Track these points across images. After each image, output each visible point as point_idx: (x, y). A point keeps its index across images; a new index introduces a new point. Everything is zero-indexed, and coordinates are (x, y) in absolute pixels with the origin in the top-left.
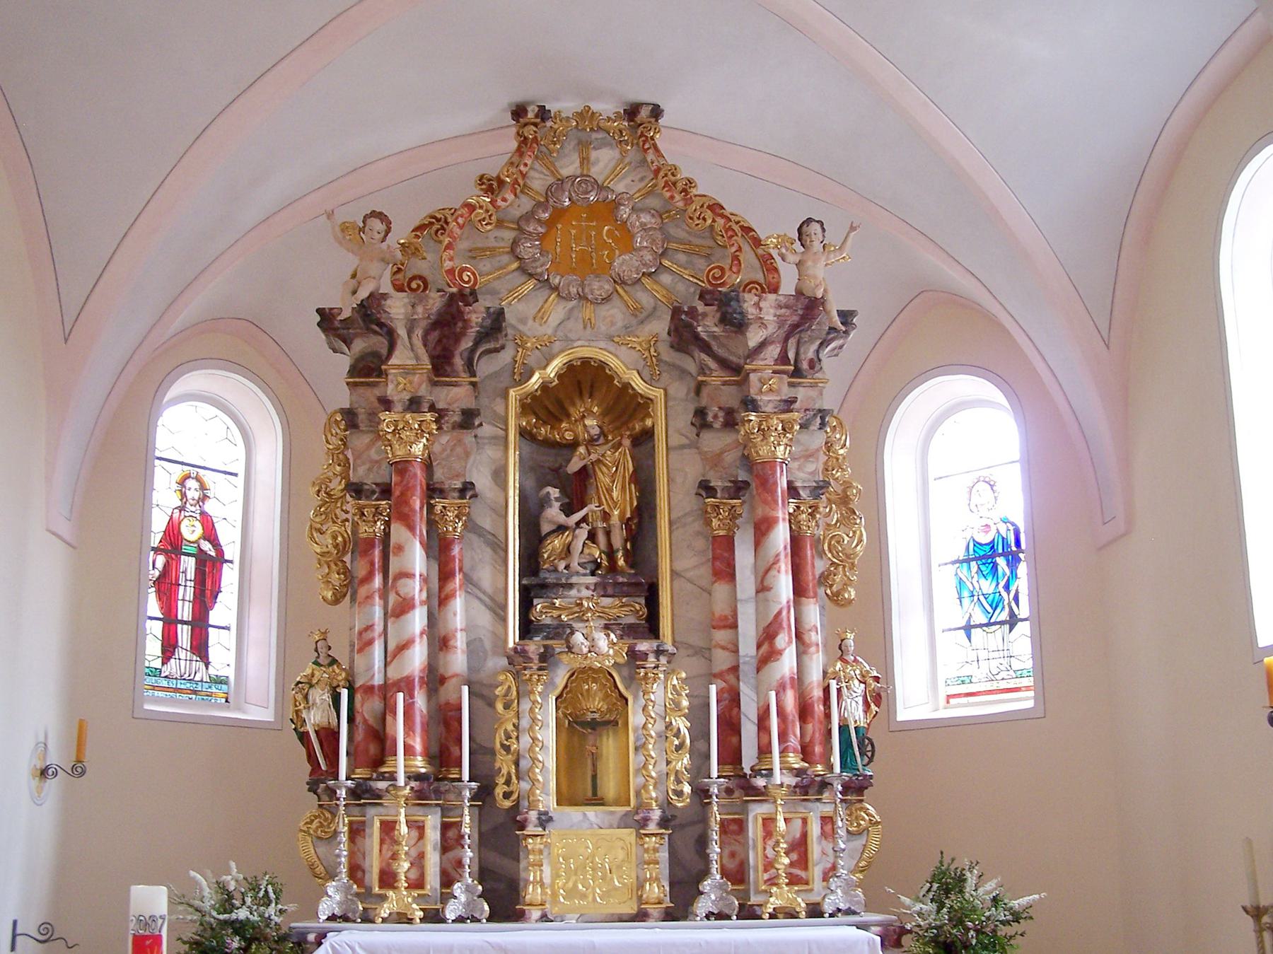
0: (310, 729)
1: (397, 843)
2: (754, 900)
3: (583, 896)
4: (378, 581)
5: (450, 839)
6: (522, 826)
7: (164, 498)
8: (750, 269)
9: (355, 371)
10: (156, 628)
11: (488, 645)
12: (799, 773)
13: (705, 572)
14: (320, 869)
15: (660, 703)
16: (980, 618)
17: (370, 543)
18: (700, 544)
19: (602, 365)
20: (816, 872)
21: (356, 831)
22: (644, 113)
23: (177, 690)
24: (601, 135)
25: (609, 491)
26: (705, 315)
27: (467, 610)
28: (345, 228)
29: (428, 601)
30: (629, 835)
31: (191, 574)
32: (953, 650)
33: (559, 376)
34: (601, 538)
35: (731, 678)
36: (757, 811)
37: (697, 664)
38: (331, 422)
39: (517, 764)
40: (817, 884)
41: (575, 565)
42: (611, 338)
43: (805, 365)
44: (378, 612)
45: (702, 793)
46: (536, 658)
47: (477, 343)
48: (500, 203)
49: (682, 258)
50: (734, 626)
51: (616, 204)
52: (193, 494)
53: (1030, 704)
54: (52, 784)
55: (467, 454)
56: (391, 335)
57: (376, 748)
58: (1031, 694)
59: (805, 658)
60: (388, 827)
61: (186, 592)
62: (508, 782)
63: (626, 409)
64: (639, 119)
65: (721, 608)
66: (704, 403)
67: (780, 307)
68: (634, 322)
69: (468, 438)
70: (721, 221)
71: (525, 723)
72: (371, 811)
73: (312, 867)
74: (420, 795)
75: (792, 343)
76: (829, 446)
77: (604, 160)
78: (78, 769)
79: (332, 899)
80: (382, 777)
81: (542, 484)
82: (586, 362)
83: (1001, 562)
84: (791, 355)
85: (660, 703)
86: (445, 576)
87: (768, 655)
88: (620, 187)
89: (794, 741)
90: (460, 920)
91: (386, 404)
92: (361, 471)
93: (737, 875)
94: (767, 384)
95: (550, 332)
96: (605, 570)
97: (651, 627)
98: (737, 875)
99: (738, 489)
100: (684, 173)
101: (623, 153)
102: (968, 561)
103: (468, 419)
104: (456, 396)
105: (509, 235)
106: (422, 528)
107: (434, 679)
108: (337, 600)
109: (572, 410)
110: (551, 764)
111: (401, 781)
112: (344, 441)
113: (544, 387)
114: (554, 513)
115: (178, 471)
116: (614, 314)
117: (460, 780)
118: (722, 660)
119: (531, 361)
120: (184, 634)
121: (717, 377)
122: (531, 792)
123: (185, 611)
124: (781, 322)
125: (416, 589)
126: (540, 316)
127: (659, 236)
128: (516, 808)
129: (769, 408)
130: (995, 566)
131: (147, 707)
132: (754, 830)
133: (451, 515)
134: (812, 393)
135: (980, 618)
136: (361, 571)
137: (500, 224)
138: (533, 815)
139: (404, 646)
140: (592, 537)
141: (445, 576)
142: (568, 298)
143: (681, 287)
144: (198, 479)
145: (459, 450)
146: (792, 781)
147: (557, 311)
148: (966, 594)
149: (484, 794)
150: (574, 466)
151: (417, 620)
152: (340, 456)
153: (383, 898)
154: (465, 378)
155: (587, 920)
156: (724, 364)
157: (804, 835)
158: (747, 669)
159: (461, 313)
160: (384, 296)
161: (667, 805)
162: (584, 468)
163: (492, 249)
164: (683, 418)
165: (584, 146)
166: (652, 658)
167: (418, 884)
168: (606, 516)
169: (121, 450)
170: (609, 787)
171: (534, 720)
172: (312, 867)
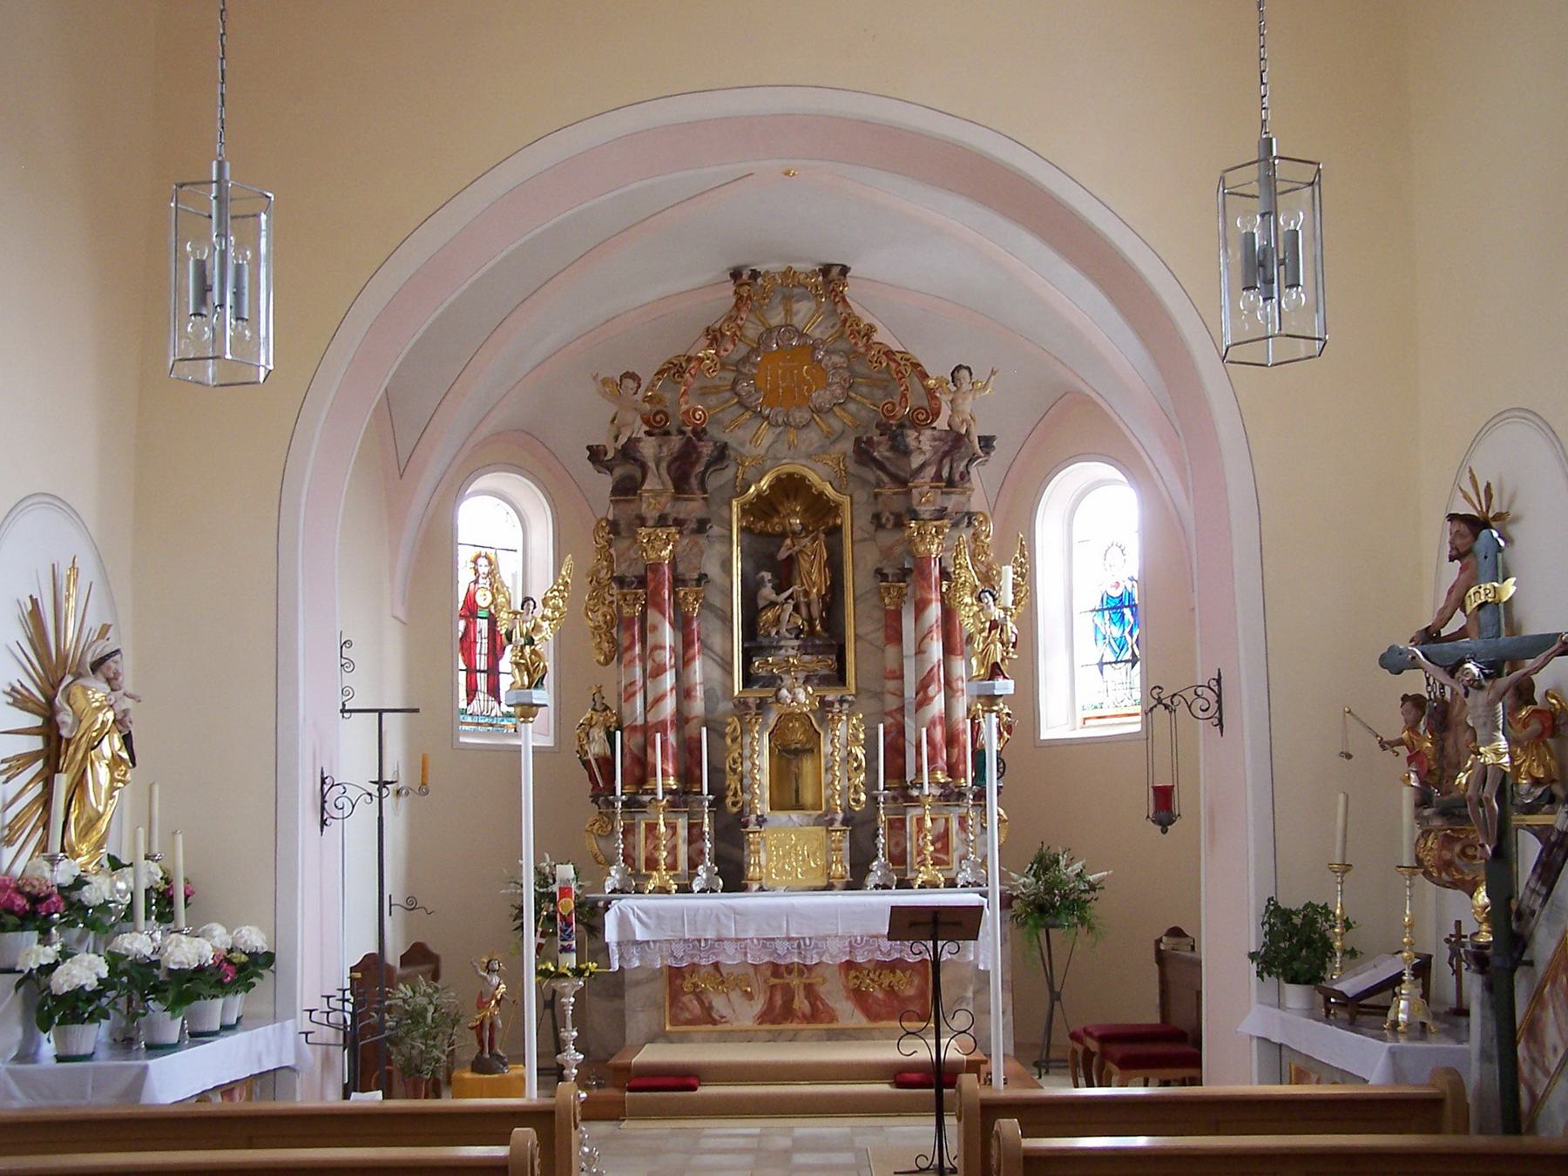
0: (590, 756)
1: (658, 838)
2: (909, 876)
3: (789, 874)
4: (637, 649)
5: (695, 835)
6: (746, 826)
7: (465, 577)
8: (916, 399)
9: (615, 491)
10: (462, 677)
11: (719, 693)
12: (943, 786)
13: (879, 637)
14: (601, 858)
15: (844, 740)
16: (1110, 657)
17: (631, 621)
18: (878, 614)
19: (803, 478)
20: (955, 856)
21: (629, 831)
22: (835, 271)
23: (478, 724)
24: (801, 290)
25: (809, 574)
26: (879, 443)
27: (703, 667)
28: (605, 382)
29: (676, 666)
30: (821, 830)
31: (485, 633)
32: (1088, 678)
33: (770, 487)
34: (804, 610)
35: (899, 717)
36: (912, 814)
37: (872, 705)
38: (598, 527)
39: (741, 781)
40: (955, 865)
41: (783, 631)
42: (809, 456)
43: (957, 477)
44: (638, 671)
45: (873, 800)
46: (753, 707)
47: (707, 469)
48: (722, 353)
49: (864, 390)
50: (901, 677)
51: (814, 348)
52: (484, 569)
53: (1138, 728)
54: (402, 800)
55: (702, 552)
56: (644, 467)
57: (641, 771)
58: (1139, 718)
59: (954, 701)
60: (652, 828)
61: (482, 646)
62: (735, 794)
63: (821, 511)
64: (832, 276)
65: (891, 664)
66: (880, 508)
67: (935, 440)
68: (827, 442)
69: (702, 540)
70: (893, 365)
71: (747, 752)
72: (638, 817)
73: (595, 857)
74: (672, 804)
75: (947, 462)
76: (976, 537)
77: (803, 310)
78: (423, 788)
79: (613, 879)
80: (646, 792)
81: (759, 569)
82: (790, 476)
83: (1127, 611)
84: (945, 474)
85: (844, 740)
86: (687, 644)
87: (923, 701)
88: (817, 334)
89: (941, 763)
90: (702, 891)
91: (642, 521)
92: (624, 567)
93: (898, 859)
94: (926, 498)
95: (763, 452)
96: (808, 640)
97: (840, 678)
98: (898, 859)
99: (904, 574)
100: (867, 319)
101: (819, 304)
102: (1102, 610)
103: (702, 526)
104: (692, 508)
105: (730, 376)
106: (669, 611)
107: (681, 719)
108: (607, 662)
109: (780, 508)
110: (766, 781)
111: (660, 796)
112: (610, 542)
113: (759, 495)
114: (767, 592)
115: (474, 552)
116: (813, 437)
117: (701, 793)
118: (892, 703)
119: (748, 476)
120: (482, 680)
121: (889, 489)
122: (752, 801)
123: (482, 662)
124: (935, 450)
125: (667, 657)
126: (755, 438)
127: (846, 375)
128: (741, 811)
129: (927, 516)
130: (1123, 615)
131: (462, 739)
132: (910, 826)
133: (691, 599)
134: (963, 499)
135: (1110, 657)
136: (626, 643)
137: (723, 366)
138: (753, 817)
139: (660, 699)
140: (796, 608)
141: (687, 644)
142: (778, 425)
143: (863, 413)
144: (486, 557)
145: (695, 550)
146: (937, 792)
147: (767, 436)
148: (1100, 637)
149: (718, 803)
150: (783, 554)
151: (669, 679)
152: (605, 554)
153: (649, 877)
154: (699, 495)
155: (790, 889)
156: (895, 478)
157: (947, 830)
158: (910, 707)
159: (695, 447)
160: (639, 440)
161: (848, 809)
162: (790, 557)
163: (717, 387)
164: (864, 520)
165: (788, 299)
166: (837, 705)
167: (672, 866)
168: (807, 594)
169: (437, 543)
170: (808, 796)
171: (753, 751)
172: (595, 857)
